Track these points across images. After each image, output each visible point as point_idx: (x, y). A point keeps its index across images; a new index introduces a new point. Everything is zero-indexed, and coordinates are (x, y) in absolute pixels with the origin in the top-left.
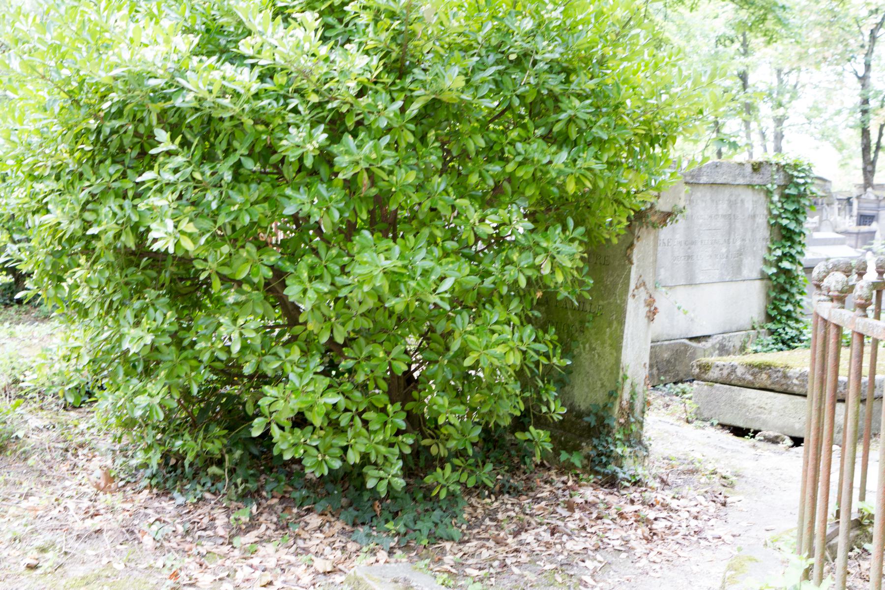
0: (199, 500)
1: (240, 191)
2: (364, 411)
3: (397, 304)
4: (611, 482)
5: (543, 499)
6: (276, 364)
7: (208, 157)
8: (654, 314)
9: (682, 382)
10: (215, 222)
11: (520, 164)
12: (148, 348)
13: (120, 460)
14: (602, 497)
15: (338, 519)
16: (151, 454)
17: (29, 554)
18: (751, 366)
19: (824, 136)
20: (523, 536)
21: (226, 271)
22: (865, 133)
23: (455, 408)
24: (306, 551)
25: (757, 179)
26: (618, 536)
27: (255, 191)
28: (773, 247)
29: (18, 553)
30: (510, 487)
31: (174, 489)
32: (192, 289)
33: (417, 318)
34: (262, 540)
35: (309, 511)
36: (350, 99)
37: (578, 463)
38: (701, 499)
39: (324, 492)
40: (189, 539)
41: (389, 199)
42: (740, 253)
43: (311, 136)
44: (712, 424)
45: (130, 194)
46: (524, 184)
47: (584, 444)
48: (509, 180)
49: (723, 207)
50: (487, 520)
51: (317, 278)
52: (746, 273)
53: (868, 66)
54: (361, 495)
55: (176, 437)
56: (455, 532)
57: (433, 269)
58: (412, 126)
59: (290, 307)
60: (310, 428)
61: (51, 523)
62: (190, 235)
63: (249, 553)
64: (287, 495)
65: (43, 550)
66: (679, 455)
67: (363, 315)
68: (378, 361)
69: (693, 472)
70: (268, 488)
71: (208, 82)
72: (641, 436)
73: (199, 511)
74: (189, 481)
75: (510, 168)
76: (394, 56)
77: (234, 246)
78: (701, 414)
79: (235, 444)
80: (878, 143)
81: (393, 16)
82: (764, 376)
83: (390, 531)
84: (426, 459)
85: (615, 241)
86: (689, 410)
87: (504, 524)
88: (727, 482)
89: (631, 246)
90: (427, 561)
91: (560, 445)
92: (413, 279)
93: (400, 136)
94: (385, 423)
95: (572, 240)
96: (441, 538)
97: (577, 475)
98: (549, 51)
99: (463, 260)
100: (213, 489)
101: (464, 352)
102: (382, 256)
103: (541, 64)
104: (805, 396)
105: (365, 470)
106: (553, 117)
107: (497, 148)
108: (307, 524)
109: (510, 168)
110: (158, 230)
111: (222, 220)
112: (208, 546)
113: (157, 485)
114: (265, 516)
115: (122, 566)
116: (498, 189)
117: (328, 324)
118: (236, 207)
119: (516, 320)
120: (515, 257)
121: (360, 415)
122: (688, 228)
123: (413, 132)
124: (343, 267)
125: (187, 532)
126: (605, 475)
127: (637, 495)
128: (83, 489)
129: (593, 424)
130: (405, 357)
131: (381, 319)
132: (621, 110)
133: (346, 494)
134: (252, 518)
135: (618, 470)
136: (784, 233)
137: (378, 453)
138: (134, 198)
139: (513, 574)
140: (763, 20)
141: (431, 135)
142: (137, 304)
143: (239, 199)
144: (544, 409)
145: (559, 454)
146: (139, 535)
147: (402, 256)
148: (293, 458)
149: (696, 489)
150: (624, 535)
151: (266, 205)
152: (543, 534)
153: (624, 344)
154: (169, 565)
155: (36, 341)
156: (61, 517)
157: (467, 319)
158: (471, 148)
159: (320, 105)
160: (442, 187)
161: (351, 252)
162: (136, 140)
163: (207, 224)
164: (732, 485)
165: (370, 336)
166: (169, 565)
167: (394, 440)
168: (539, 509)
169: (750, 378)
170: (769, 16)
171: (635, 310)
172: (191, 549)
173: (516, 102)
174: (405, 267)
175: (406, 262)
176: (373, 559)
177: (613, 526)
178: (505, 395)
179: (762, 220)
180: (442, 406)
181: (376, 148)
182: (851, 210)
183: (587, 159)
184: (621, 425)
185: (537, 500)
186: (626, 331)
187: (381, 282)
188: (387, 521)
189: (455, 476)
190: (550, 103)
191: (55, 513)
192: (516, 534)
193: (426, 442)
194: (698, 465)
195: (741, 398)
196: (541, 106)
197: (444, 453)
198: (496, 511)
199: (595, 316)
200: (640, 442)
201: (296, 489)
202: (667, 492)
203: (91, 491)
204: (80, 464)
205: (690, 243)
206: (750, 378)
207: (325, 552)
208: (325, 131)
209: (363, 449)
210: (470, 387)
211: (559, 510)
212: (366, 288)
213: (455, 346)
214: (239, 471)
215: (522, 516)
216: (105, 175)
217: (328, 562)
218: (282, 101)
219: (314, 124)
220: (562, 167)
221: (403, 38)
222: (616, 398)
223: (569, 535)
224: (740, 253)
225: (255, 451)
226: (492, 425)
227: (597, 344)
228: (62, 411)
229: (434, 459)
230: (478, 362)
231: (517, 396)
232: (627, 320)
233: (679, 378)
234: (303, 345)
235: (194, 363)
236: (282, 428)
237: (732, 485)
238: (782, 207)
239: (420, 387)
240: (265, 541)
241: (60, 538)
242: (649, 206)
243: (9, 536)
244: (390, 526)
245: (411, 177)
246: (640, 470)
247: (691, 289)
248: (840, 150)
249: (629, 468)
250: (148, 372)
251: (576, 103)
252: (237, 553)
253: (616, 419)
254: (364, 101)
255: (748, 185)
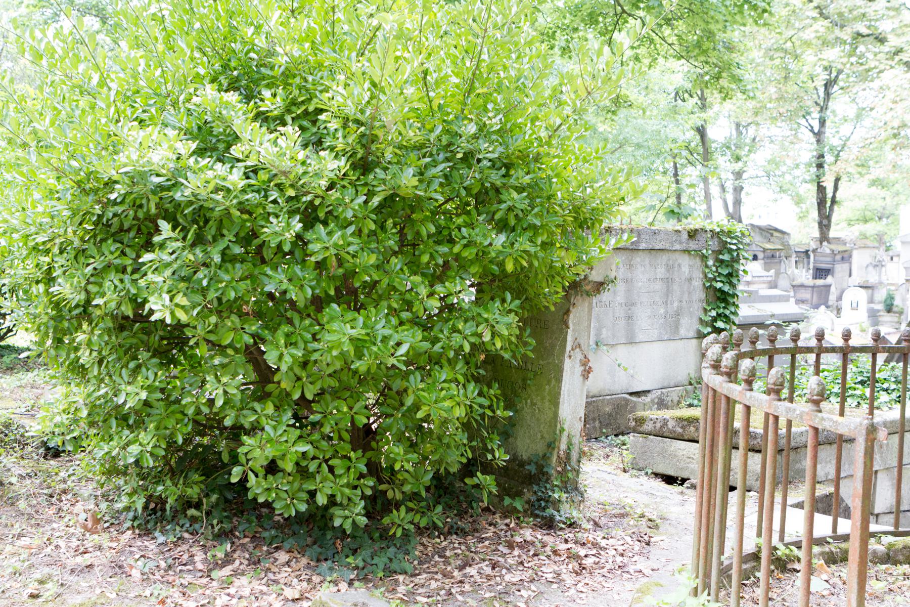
0: (179, 539)
1: (227, 271)
2: (330, 458)
3: (360, 366)
4: (549, 525)
5: (487, 539)
6: (253, 418)
7: (199, 240)
8: (589, 373)
9: (623, 434)
10: (204, 296)
11: (465, 246)
12: (142, 403)
13: (104, 505)
14: (540, 537)
15: (303, 555)
16: (135, 498)
17: (31, 585)
18: (681, 419)
19: (782, 190)
20: (468, 570)
21: (212, 337)
22: (821, 189)
23: (409, 456)
24: (276, 582)
25: (693, 245)
26: (551, 570)
27: (239, 270)
28: (709, 308)
29: (19, 585)
30: (458, 529)
31: (155, 529)
32: (169, 347)
33: (376, 377)
34: (236, 573)
35: (277, 549)
36: (320, 193)
37: (520, 508)
38: (628, 539)
39: (291, 532)
40: (171, 573)
41: (353, 277)
42: (678, 314)
43: (288, 224)
44: (646, 474)
45: (129, 269)
46: (469, 263)
47: (525, 490)
48: (456, 260)
49: (661, 272)
50: (436, 556)
51: (291, 344)
52: (683, 332)
53: (822, 123)
54: (324, 535)
55: (157, 483)
56: (409, 568)
57: (391, 336)
58: (373, 216)
59: (263, 366)
60: (281, 474)
61: (45, 559)
62: (183, 307)
63: (226, 584)
64: (258, 535)
65: (41, 582)
66: (614, 501)
67: (330, 375)
68: (338, 414)
69: (623, 516)
70: (241, 528)
71: (206, 180)
72: (577, 482)
73: (179, 549)
74: (169, 523)
75: (456, 249)
76: (359, 156)
77: (221, 317)
78: (637, 464)
79: (213, 491)
80: (834, 197)
81: (359, 123)
82: (692, 429)
83: (350, 564)
84: (383, 504)
85: (553, 308)
86: (626, 460)
87: (451, 560)
88: (653, 525)
89: (567, 312)
90: (383, 589)
91: (505, 491)
92: (375, 344)
93: (363, 224)
94: (349, 468)
95: (510, 311)
96: (395, 572)
97: (518, 518)
98: (489, 150)
99: (416, 328)
100: (191, 529)
101: (416, 407)
102: (348, 326)
103: (485, 162)
104: (697, 442)
105: (331, 511)
106: (495, 207)
107: (445, 232)
108: (276, 560)
109: (456, 249)
110: (156, 303)
111: (212, 295)
112: (188, 578)
113: (139, 526)
114: (238, 553)
115: (114, 596)
116: (446, 265)
117: (299, 383)
118: (224, 284)
119: (461, 379)
120: (460, 326)
121: (326, 461)
122: (628, 291)
123: (375, 222)
124: (314, 335)
125: (170, 567)
126: (543, 518)
127: (571, 535)
128: (72, 530)
129: (534, 471)
130: (365, 411)
131: (345, 378)
132: (552, 201)
133: (314, 534)
134: (227, 555)
135: (556, 513)
136: (719, 295)
137: (342, 494)
138: (133, 273)
139: (457, 601)
140: (718, 77)
141: (390, 222)
142: (132, 365)
143: (227, 277)
144: (490, 457)
145: (503, 500)
146: (127, 569)
147: (365, 326)
148: (266, 501)
149: (624, 530)
150: (556, 568)
151: (248, 282)
152: (485, 568)
153: (561, 400)
154: (156, 593)
155: (7, 393)
156: (54, 554)
157: (419, 378)
158: (424, 233)
159: (296, 198)
160: (398, 267)
161: (321, 322)
162: (134, 222)
163: (198, 298)
164: (657, 527)
165: (336, 394)
166: (156, 593)
167: (356, 483)
168: (483, 547)
169: (680, 430)
170: (724, 75)
171: (571, 369)
172: (174, 581)
173: (463, 193)
174: (368, 334)
175: (369, 331)
176: (336, 589)
177: (547, 562)
178: (453, 444)
179: (698, 283)
180: (398, 454)
181: (343, 237)
182: (809, 263)
183: (523, 243)
184: (559, 472)
185: (481, 540)
186: (563, 388)
187: (348, 347)
188: (347, 557)
189: (410, 516)
190: (492, 193)
191: (48, 550)
192: (461, 568)
193: (383, 487)
194: (628, 509)
195: (672, 449)
196: (485, 196)
197: (399, 496)
198: (445, 549)
199: (536, 374)
200: (576, 489)
201: (265, 529)
202: (599, 533)
203: (79, 530)
204: (65, 508)
205: (630, 304)
206: (680, 430)
207: (293, 584)
208: (300, 221)
209: (330, 492)
210: (422, 438)
211: (501, 548)
212: (335, 353)
213: (409, 401)
214: (215, 513)
215: (467, 553)
216: (107, 253)
217: (296, 591)
218: (263, 193)
219: (291, 213)
220: (501, 248)
221: (368, 141)
222: (554, 449)
223: (508, 569)
224: (678, 314)
225: (229, 496)
226: (442, 470)
227: (537, 400)
228: (42, 459)
229: (389, 502)
230: (429, 415)
231: (465, 445)
232: (564, 378)
233: (620, 430)
234: (276, 400)
235: (179, 416)
236: (257, 476)
237: (657, 527)
238: (717, 271)
239: (378, 438)
240: (239, 574)
241: (55, 571)
242: (582, 277)
243: (10, 570)
244: (350, 560)
245: (373, 259)
246: (575, 513)
247: (630, 347)
248: (797, 203)
249: (568, 511)
250: (139, 424)
251: (515, 195)
252: (215, 584)
253: (554, 467)
254: (334, 195)
255: (685, 251)
